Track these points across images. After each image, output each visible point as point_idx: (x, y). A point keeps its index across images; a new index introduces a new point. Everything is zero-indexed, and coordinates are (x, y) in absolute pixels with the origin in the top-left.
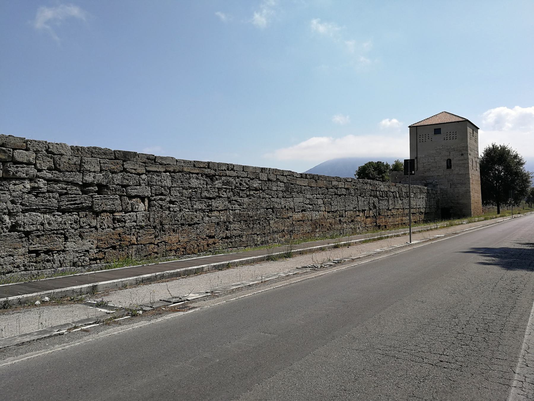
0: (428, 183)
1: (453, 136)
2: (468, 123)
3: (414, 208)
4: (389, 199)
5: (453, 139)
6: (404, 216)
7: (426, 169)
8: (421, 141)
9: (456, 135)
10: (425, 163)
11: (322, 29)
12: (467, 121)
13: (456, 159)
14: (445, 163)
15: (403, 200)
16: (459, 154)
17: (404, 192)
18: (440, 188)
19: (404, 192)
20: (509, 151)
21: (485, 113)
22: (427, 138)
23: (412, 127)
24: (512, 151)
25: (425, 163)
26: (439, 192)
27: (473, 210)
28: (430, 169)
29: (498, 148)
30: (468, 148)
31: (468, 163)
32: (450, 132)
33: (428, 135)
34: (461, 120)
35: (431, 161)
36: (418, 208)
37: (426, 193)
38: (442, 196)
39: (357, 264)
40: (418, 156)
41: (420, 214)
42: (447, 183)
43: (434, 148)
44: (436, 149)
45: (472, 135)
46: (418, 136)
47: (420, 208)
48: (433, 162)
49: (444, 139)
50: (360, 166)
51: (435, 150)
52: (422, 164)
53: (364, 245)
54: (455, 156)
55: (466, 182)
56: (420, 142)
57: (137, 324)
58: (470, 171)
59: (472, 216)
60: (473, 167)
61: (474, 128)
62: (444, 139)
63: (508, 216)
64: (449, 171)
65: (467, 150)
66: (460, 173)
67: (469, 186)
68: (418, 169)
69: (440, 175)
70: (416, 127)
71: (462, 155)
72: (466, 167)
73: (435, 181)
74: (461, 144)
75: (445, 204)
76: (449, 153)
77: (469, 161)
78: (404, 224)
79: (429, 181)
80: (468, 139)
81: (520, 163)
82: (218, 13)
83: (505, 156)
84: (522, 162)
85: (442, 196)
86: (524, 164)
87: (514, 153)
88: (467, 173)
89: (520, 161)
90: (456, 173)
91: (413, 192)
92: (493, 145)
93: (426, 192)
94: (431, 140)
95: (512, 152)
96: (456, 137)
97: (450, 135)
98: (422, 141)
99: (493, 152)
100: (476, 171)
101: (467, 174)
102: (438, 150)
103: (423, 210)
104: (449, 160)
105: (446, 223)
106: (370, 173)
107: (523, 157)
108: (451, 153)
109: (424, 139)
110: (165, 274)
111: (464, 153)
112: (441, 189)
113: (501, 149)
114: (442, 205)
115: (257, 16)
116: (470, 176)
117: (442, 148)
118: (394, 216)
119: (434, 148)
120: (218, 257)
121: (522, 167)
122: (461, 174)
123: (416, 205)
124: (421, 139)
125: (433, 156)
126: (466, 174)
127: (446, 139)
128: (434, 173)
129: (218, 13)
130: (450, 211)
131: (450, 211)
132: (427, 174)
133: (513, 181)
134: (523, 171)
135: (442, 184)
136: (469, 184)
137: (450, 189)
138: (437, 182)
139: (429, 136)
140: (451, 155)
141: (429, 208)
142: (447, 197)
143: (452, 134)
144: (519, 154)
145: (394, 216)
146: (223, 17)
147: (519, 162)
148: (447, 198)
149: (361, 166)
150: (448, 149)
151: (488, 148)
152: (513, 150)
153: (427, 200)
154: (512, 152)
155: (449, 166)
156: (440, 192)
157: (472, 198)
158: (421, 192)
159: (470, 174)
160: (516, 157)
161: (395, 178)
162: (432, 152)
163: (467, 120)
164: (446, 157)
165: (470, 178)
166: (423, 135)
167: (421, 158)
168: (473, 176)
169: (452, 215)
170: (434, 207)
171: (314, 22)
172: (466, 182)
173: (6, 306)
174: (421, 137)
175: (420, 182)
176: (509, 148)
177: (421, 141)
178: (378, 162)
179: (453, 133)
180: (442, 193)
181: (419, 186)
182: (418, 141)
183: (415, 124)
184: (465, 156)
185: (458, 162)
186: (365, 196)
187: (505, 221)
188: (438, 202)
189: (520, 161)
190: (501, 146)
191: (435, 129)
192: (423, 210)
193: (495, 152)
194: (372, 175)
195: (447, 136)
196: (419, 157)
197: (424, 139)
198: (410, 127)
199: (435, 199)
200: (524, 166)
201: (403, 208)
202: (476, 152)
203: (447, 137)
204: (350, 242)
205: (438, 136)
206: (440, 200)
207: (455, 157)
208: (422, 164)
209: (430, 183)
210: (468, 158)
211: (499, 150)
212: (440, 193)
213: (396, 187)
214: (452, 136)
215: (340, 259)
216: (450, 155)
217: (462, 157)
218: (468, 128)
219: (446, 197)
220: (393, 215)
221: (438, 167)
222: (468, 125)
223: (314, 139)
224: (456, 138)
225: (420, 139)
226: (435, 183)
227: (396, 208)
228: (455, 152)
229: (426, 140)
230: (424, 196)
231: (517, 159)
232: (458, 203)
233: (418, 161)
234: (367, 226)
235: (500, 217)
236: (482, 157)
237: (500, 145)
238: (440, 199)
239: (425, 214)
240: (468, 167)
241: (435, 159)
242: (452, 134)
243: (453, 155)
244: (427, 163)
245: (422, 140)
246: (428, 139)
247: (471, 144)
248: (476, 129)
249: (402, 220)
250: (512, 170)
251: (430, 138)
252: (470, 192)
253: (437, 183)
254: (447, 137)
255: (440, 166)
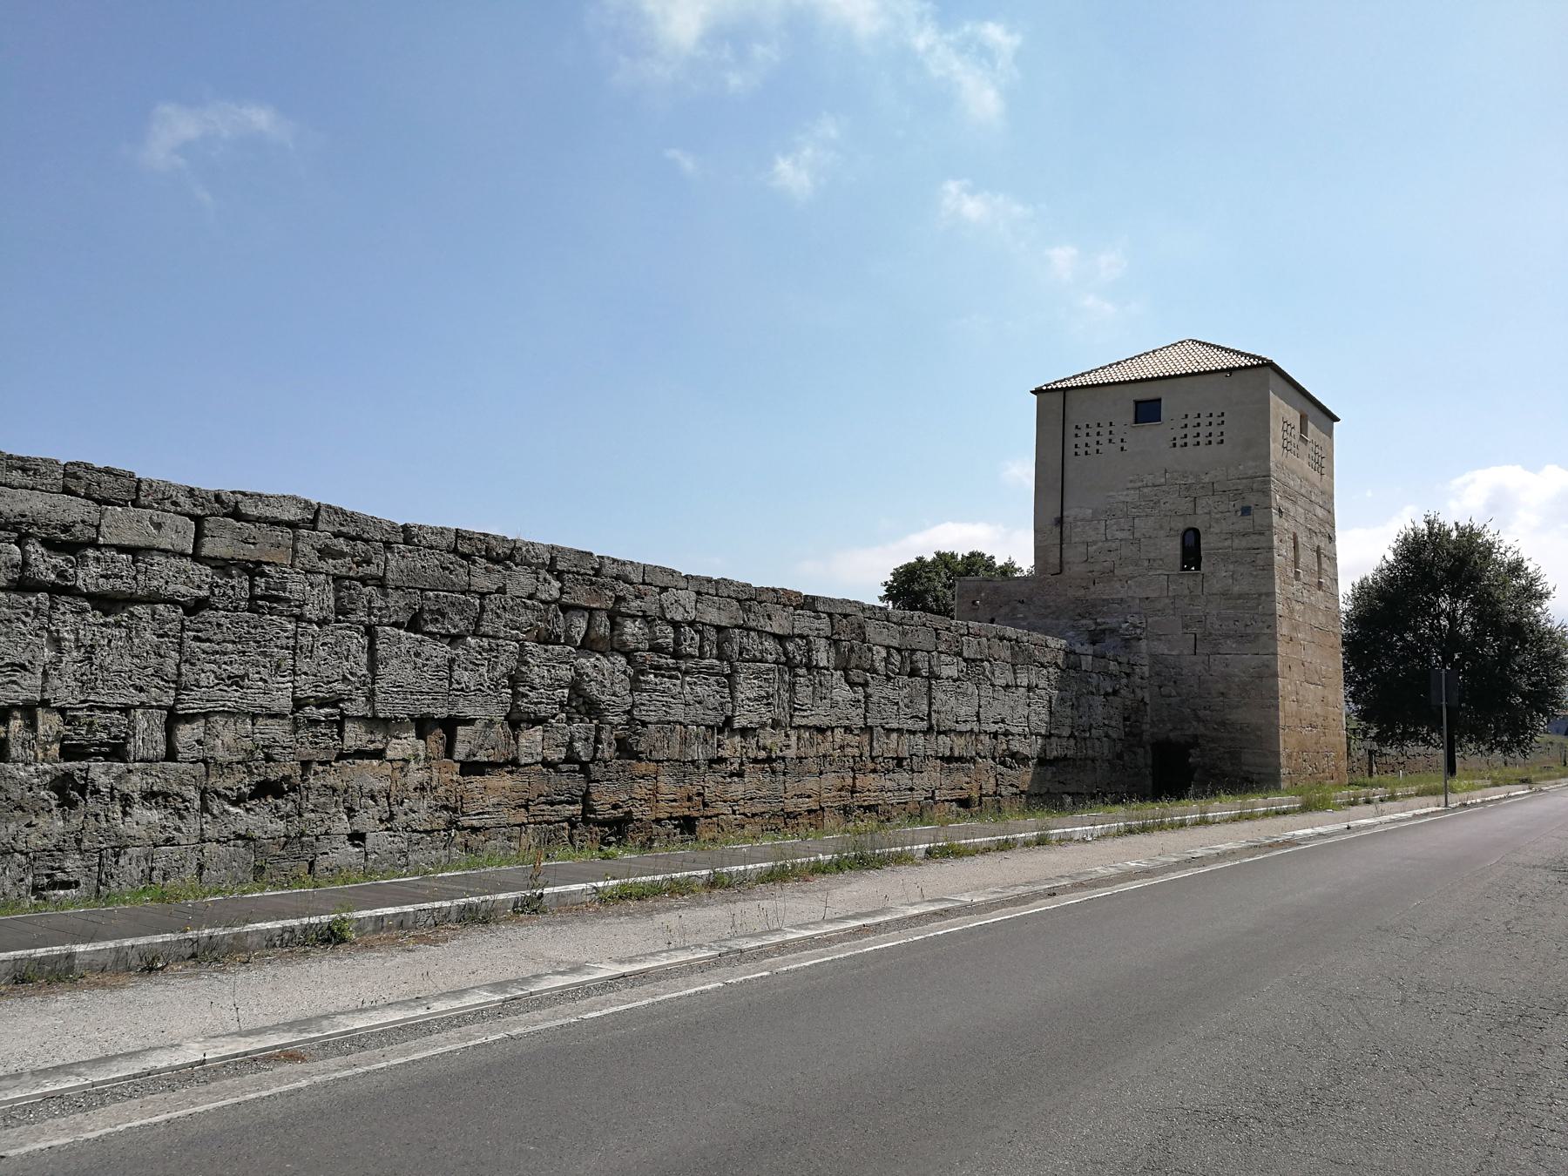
0: (1105, 629)
1: (1210, 429)
2: (1274, 379)
3: (961, 733)
4: (734, 671)
5: (1210, 442)
6: (874, 771)
7: (1097, 567)
8: (1081, 451)
9: (1222, 428)
10: (1095, 543)
11: (973, 208)
12: (1269, 370)
13: (1217, 531)
14: (1174, 548)
15: (865, 685)
16: (1231, 508)
17: (888, 648)
18: (1151, 655)
19: (888, 648)
20: (1489, 547)
21: (1458, 481)
22: (1104, 439)
23: (1047, 390)
24: (1500, 547)
25: (1095, 543)
26: (1146, 669)
27: (1289, 756)
28: (1112, 571)
29: (1449, 533)
30: (1269, 482)
31: (1271, 548)
32: (1199, 416)
33: (1111, 424)
34: (1244, 362)
35: (1120, 535)
36: (995, 735)
37: (1057, 666)
38: (1160, 687)
39: (765, 974)
40: (1065, 513)
41: (1003, 763)
42: (1180, 633)
43: (1131, 481)
44: (1140, 484)
45: (1296, 432)
46: (1071, 430)
47: (1007, 733)
48: (1125, 540)
49: (1175, 445)
50: (898, 567)
51: (1135, 489)
52: (1082, 549)
53: (1234, 826)
54: (1217, 516)
55: (1262, 628)
56: (1076, 454)
57: (320, 1064)
58: (1277, 581)
59: (1284, 785)
60: (1297, 566)
61: (1312, 411)
62: (1175, 445)
63: (1465, 791)
64: (1188, 581)
65: (1266, 493)
66: (1236, 589)
67: (1271, 650)
68: (1066, 567)
69: (1152, 595)
70: (1062, 393)
71: (1246, 511)
72: (1262, 563)
73: (1130, 620)
74: (1241, 467)
75: (1169, 726)
76: (1191, 505)
77: (1275, 537)
78: (869, 808)
79: (1108, 620)
80: (1275, 447)
81: (1532, 593)
82: (672, 153)
83: (1476, 563)
84: (1540, 588)
85: (1160, 687)
86: (1546, 595)
87: (1509, 554)
88: (1264, 590)
89: (1531, 585)
90: (1217, 587)
91: (959, 654)
92: (1428, 523)
93: (1060, 662)
94: (1122, 449)
95: (1502, 550)
96: (1222, 433)
97: (1199, 425)
98: (1086, 453)
99: (1430, 546)
100: (1314, 590)
101: (1263, 597)
102: (1145, 490)
103: (1030, 748)
104: (1192, 532)
105: (1119, 816)
106: (927, 591)
107: (1542, 572)
108: (1202, 502)
109: (1092, 441)
110: (748, 873)
111: (1252, 505)
112: (1156, 659)
113: (1462, 534)
114: (1156, 730)
115: (783, 165)
116: (1279, 607)
117: (1163, 480)
118: (779, 766)
119: (1131, 481)
120: (380, 887)
121: (1538, 610)
122: (1240, 596)
123: (979, 720)
124: (1081, 441)
125: (1126, 516)
126: (1260, 595)
127: (1179, 442)
128: (1129, 587)
129: (672, 153)
130: (1190, 755)
131: (1190, 755)
132: (1100, 591)
133: (1506, 655)
134: (1543, 621)
135: (1159, 637)
136: (1273, 637)
137: (1194, 658)
138: (1136, 627)
139: (1111, 428)
140: (1199, 511)
141: (1072, 736)
142: (1179, 695)
143: (1204, 420)
144: (1525, 559)
145: (779, 766)
146: (688, 164)
147: (1526, 589)
148: (1179, 698)
149: (901, 568)
150: (1188, 487)
151: (1412, 533)
152: (1507, 543)
153: (1062, 700)
154: (1502, 550)
155: (1191, 554)
156: (1150, 670)
157: (1287, 707)
158: (1021, 657)
159: (1279, 597)
160: (1516, 568)
161: (974, 603)
162: (1122, 498)
163: (1270, 365)
164: (1182, 518)
165: (1278, 613)
166: (1088, 426)
167: (1079, 523)
168: (1298, 607)
169: (1196, 775)
170: (1107, 736)
171: (952, 187)
172: (1262, 628)
173: (23, 978)
174: (1083, 433)
175: (1071, 623)
176: (1489, 537)
177: (1081, 451)
178: (973, 554)
179: (1210, 419)
180: (1158, 674)
181: (1010, 632)
182: (1070, 451)
183: (1061, 381)
184: (1257, 515)
185: (1227, 543)
186: (475, 634)
187: (1359, 828)
188: (1131, 717)
189: (1531, 585)
190: (1461, 524)
191: (1137, 403)
192: (1030, 748)
193: (1437, 547)
194: (936, 599)
195: (1185, 431)
196: (1071, 519)
197: (1092, 441)
198: (1037, 392)
199: (1117, 701)
200: (1547, 604)
201: (868, 729)
202: (1320, 512)
203: (1186, 436)
204: (964, 841)
205: (1148, 431)
206: (1148, 708)
207: (1217, 521)
208: (1082, 549)
209: (1110, 629)
210: (1270, 526)
211: (1454, 542)
212: (1151, 676)
213: (816, 611)
214: (1204, 430)
215: (923, 900)
216: (1195, 513)
217: (1243, 524)
218: (1309, 422)
219: (1174, 693)
220: (769, 760)
221: (1146, 563)
222: (1272, 383)
223: (950, 526)
224: (1222, 441)
225: (1076, 441)
226: (1127, 630)
227: (797, 721)
228: (1217, 498)
229: (1099, 447)
230: (1044, 680)
231: (1518, 577)
232: (1223, 724)
233: (1064, 536)
234: (465, 821)
235: (1417, 795)
236: (1387, 562)
237: (1456, 524)
238: (1147, 700)
239: (1036, 765)
240: (1269, 566)
241: (1132, 529)
242: (1204, 420)
243: (1209, 513)
244: (1100, 544)
245: (1087, 445)
246: (1110, 441)
247: (1293, 472)
248: (1329, 420)
249: (853, 792)
250: (1500, 614)
251: (1117, 440)
252: (1275, 675)
253: (1138, 631)
254: (1186, 436)
255: (1152, 555)
